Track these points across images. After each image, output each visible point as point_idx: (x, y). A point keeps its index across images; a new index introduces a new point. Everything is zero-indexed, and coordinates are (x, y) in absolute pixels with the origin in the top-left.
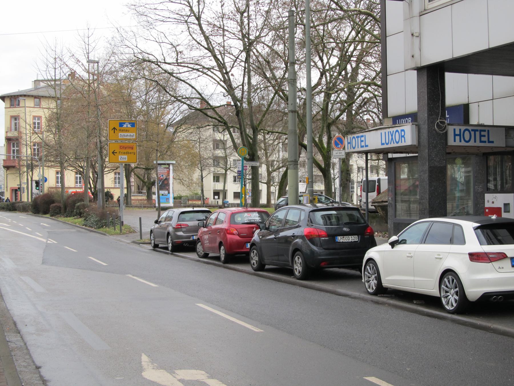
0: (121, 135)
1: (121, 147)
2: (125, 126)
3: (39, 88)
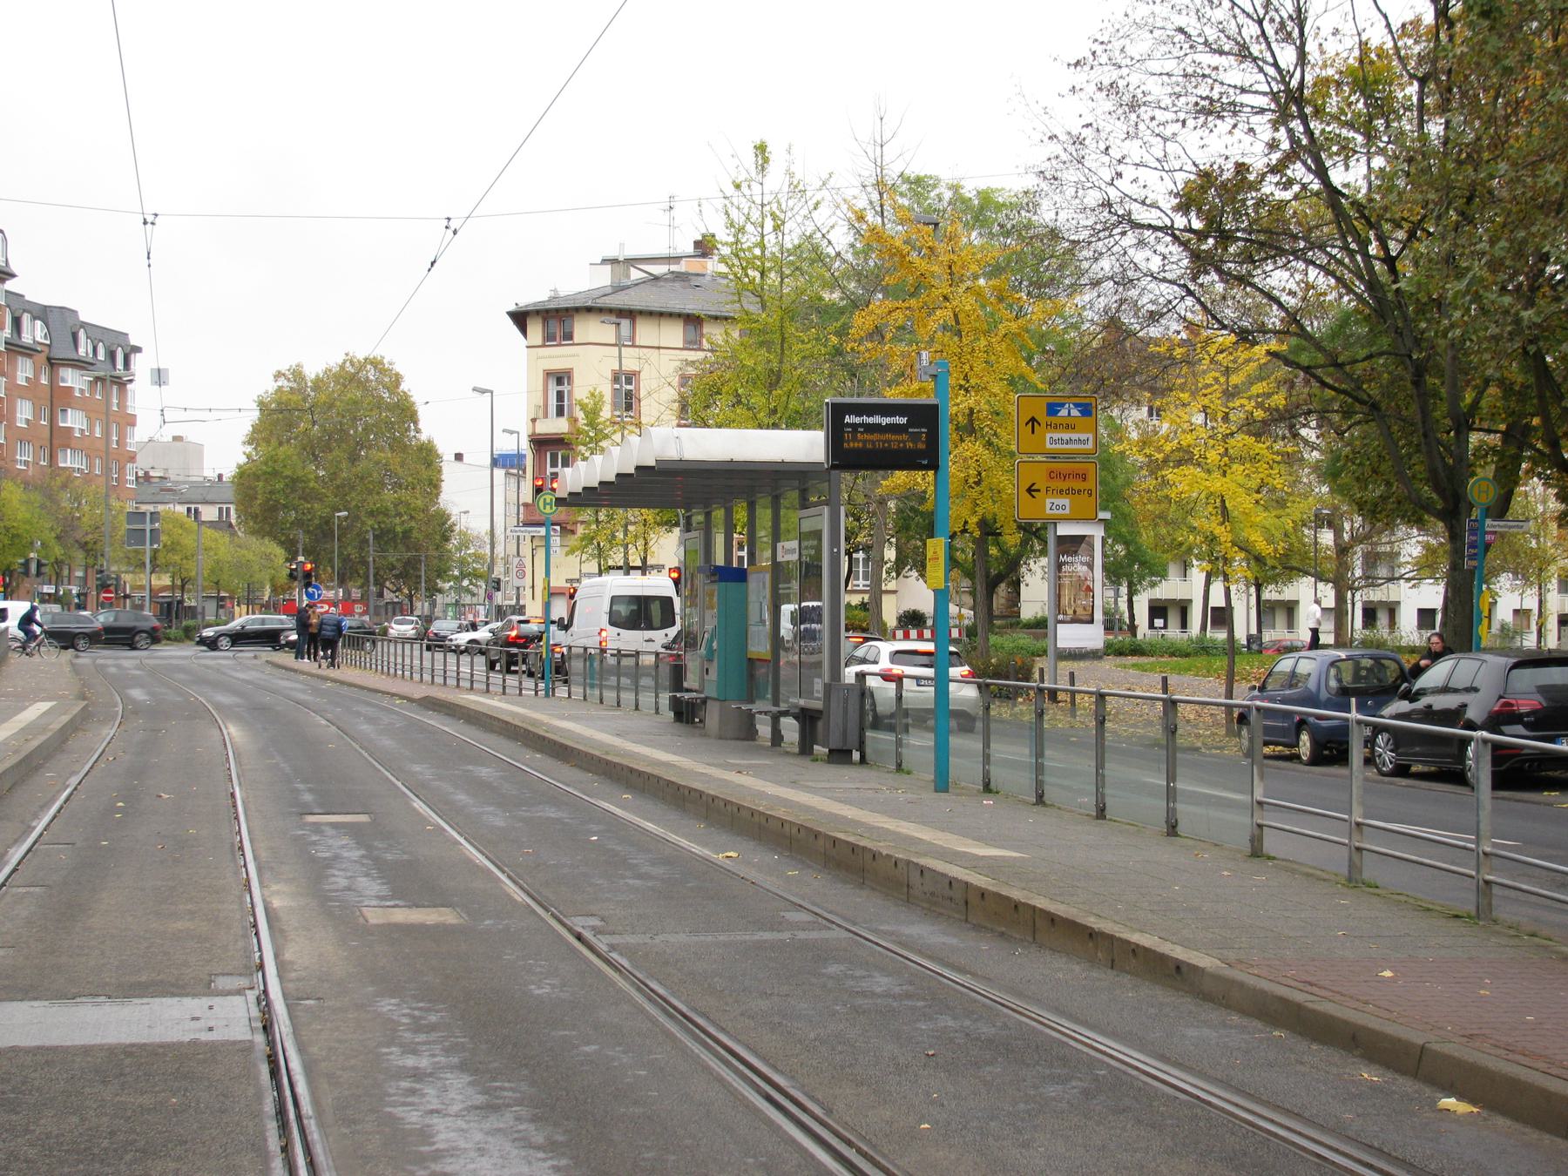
0: (1053, 440)
1: (1052, 475)
2: (1064, 412)
3: (628, 287)
